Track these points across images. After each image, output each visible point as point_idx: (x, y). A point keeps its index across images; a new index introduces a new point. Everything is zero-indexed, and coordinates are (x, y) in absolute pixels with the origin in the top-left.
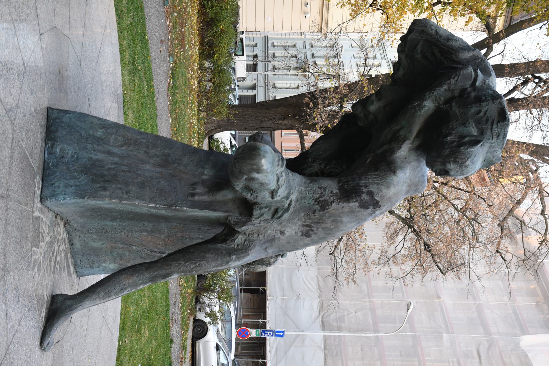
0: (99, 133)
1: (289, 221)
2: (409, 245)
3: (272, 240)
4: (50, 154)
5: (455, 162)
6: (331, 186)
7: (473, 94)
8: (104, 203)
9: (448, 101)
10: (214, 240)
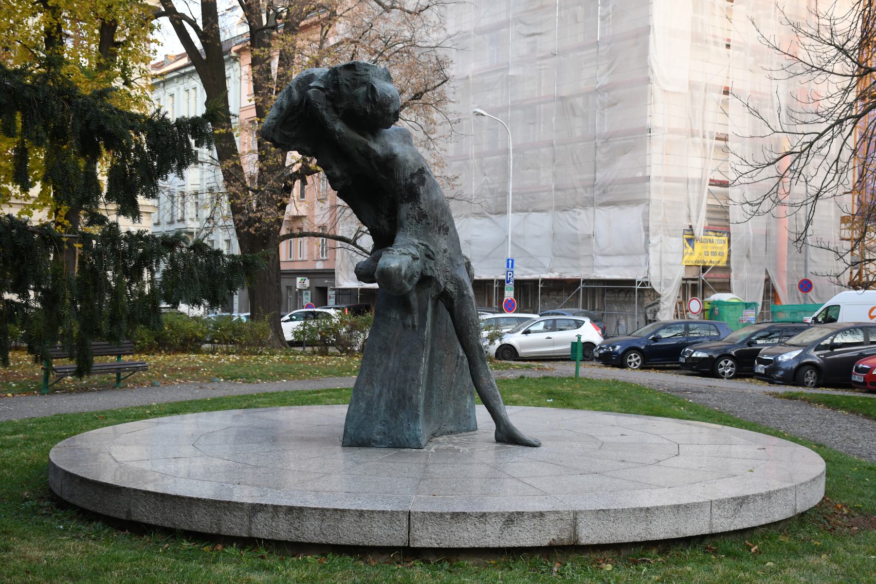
0: (363, 405)
1: (435, 246)
2: (413, 115)
3: (451, 260)
4: (381, 443)
5: (388, 106)
6: (405, 209)
7: (332, 90)
8: (422, 399)
9: (336, 110)
10: (451, 310)
